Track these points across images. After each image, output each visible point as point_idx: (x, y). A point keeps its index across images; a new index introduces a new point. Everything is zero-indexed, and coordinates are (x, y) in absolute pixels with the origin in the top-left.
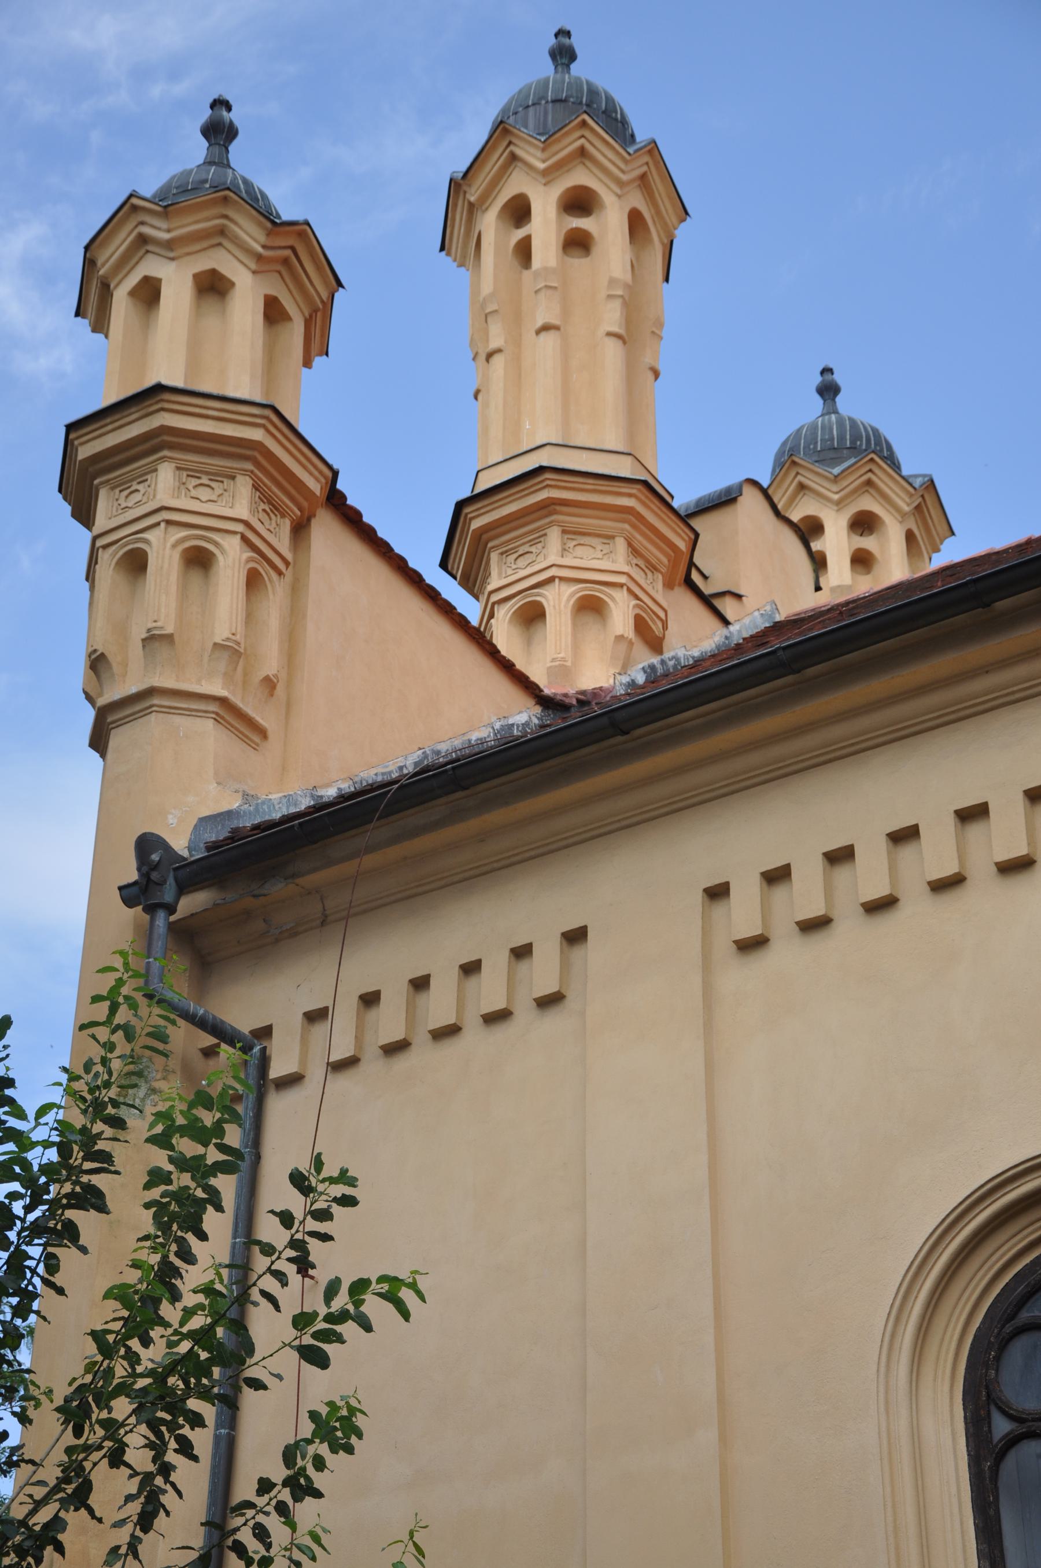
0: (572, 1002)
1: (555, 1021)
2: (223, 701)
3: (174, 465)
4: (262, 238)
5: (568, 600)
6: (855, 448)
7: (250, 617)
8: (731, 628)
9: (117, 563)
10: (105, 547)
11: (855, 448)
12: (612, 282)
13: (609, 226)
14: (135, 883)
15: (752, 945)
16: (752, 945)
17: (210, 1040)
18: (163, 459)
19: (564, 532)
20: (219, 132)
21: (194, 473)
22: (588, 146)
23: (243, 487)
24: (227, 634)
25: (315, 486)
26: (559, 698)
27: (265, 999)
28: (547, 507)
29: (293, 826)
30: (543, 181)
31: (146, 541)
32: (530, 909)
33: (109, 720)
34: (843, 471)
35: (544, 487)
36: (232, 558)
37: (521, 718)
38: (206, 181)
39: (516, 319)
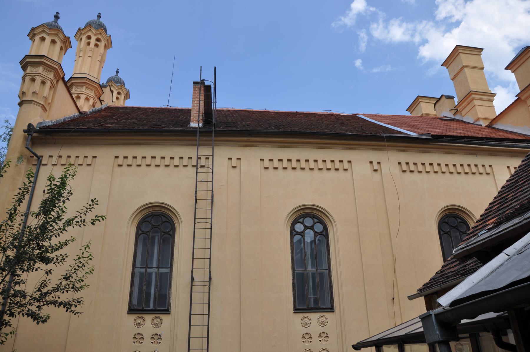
0: (92, 165)
1: (89, 168)
2: (43, 105)
7: (49, 94)
13: (102, 45)
15: (120, 166)
16: (120, 166)
17: (33, 155)
20: (57, 17)
21: (45, 69)
23: (52, 74)
25: (62, 77)
27: (44, 152)
28: (85, 83)
32: (89, 151)
36: (48, 84)
37: (76, 114)
39: (85, 53)
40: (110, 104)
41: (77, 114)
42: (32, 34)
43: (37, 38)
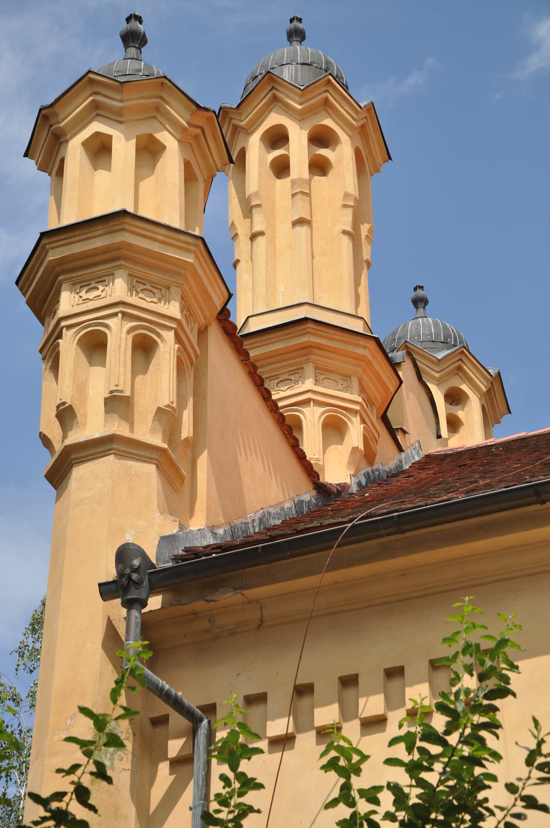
3: (128, 272)
4: (188, 117)
5: (320, 418)
6: (447, 343)
8: (403, 455)
9: (80, 340)
10: (69, 327)
11: (447, 343)
12: (347, 195)
14: (113, 582)
18: (119, 267)
19: (316, 368)
21: (141, 281)
22: (330, 98)
24: (167, 402)
26: (329, 486)
28: (307, 349)
29: (257, 548)
30: (299, 118)
31: (107, 326)
33: (73, 457)
34: (444, 358)
35: (306, 334)
36: (167, 348)
37: (306, 497)
38: (140, 70)
40: (434, 448)
41: (308, 495)
42: (46, 144)
43: (74, 152)
